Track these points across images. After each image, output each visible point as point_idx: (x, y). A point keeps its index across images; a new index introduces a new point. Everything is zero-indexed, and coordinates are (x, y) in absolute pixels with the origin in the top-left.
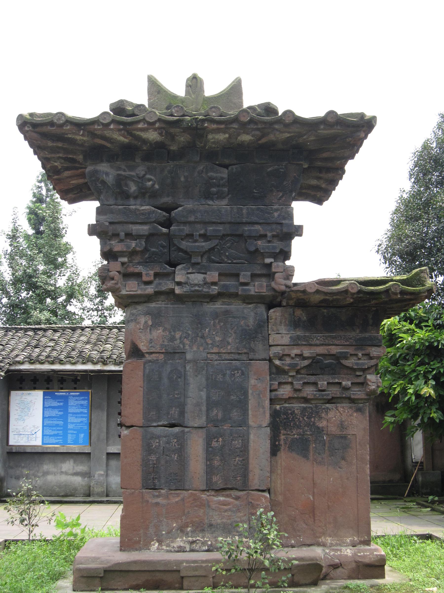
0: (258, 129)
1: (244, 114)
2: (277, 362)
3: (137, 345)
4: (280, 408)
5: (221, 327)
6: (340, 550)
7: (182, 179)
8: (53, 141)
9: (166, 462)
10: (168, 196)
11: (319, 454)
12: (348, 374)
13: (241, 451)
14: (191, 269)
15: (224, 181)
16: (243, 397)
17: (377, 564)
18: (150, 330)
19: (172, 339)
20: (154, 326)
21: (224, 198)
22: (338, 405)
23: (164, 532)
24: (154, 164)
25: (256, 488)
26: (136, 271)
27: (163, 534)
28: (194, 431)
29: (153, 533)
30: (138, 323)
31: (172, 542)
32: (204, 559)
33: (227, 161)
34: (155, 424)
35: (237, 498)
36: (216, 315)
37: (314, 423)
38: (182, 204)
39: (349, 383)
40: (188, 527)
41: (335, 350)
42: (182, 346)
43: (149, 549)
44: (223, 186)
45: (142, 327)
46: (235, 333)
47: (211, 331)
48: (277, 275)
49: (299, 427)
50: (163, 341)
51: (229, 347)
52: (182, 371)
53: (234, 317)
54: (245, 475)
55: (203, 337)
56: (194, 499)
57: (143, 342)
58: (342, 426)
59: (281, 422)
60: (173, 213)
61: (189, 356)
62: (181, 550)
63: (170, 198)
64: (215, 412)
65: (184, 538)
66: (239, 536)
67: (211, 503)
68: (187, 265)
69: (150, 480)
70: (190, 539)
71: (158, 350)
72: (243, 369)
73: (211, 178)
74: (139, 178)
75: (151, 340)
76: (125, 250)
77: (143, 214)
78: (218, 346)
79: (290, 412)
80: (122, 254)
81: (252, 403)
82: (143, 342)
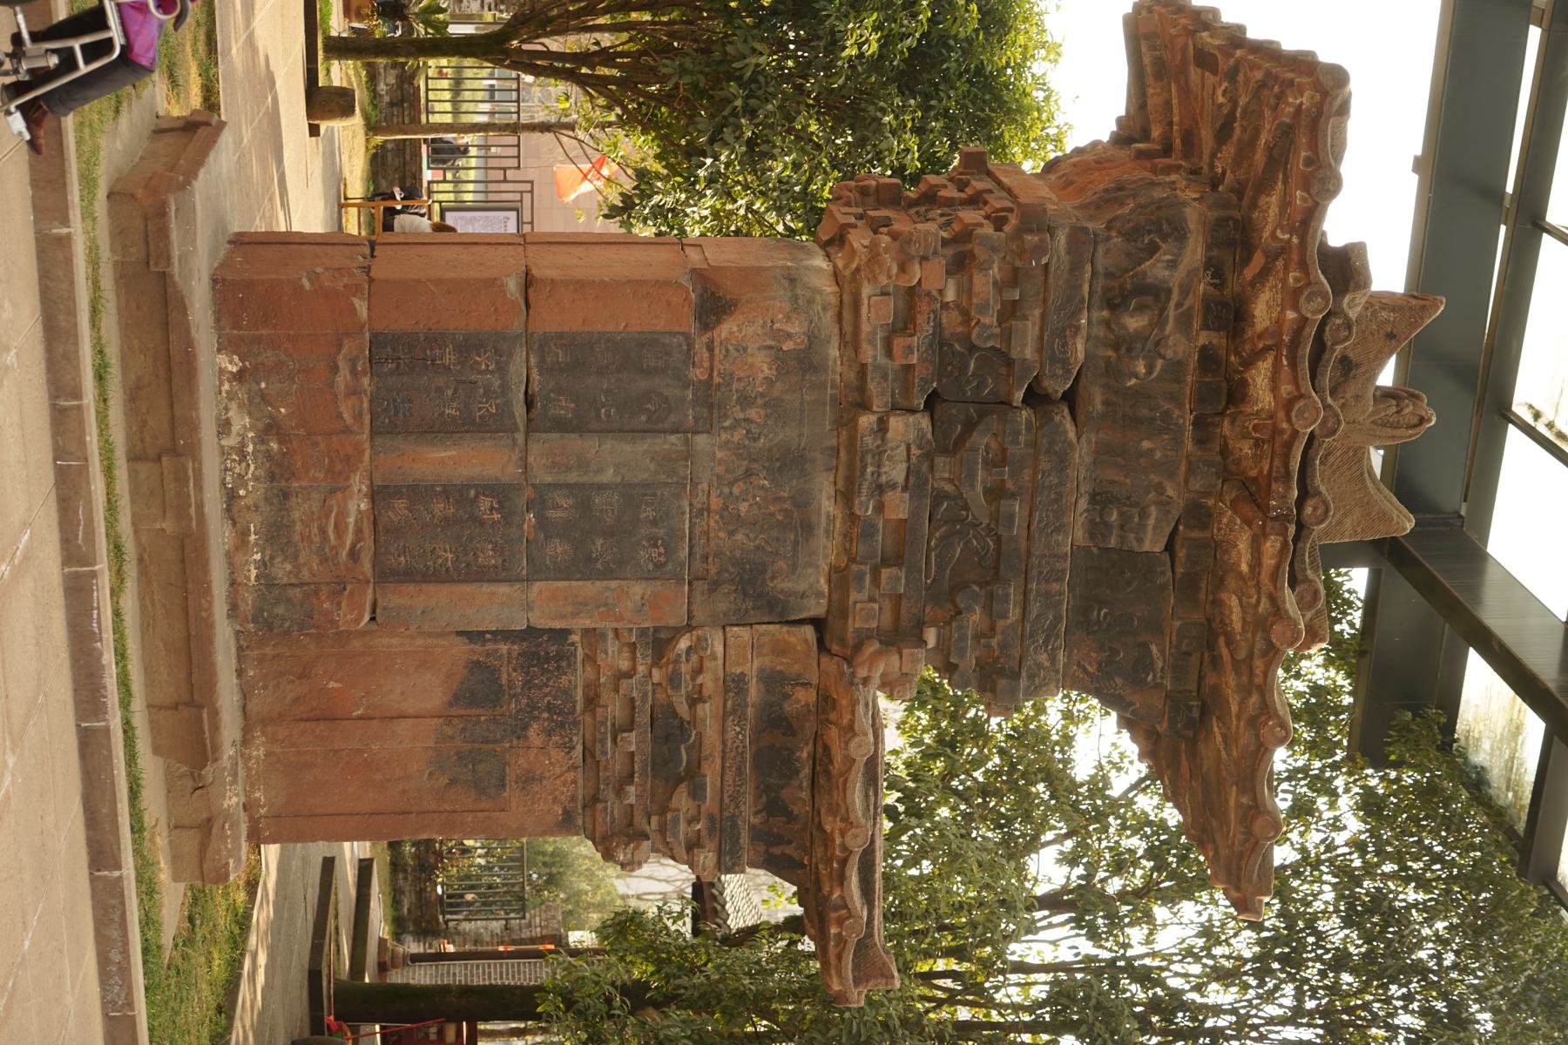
0: (1251, 656)
1: (1289, 634)
2: (684, 644)
3: (732, 313)
4: (573, 644)
5: (773, 515)
6: (234, 782)
7: (1146, 444)
8: (1270, 149)
9: (439, 390)
10: (1105, 403)
11: (463, 730)
12: (653, 795)
13: (468, 565)
14: (918, 452)
15: (1134, 543)
16: (599, 565)
17: (170, 290)
18: (771, 347)
19: (745, 401)
20: (780, 359)
21: (1092, 536)
22: (580, 770)
23: (263, 385)
24: (1189, 379)
25: (380, 603)
26: (920, 319)
27: (259, 384)
28: (515, 456)
29: (260, 359)
30: (788, 318)
31: (240, 406)
32: (206, 510)
33: (1182, 554)
34: (532, 361)
35: (354, 555)
36: (803, 502)
37: (536, 719)
38: (1083, 439)
39: (632, 800)
40: (280, 443)
41: (711, 774)
42: (727, 424)
43: (219, 351)
44: (1122, 539)
45: (777, 326)
46: (757, 548)
47: (761, 493)
48: (894, 659)
49: (528, 685)
50: (739, 379)
51: (722, 535)
52: (666, 425)
53: (796, 543)
54: (408, 576)
55: (748, 474)
56: (348, 458)
57: (740, 331)
58: (528, 780)
59: (540, 645)
60: (1063, 417)
61: (701, 441)
62: (224, 427)
63: (1099, 406)
64: (564, 503)
65: (250, 435)
66: (263, 559)
67: (339, 495)
68: (929, 442)
69: (394, 350)
70: (250, 448)
71: (718, 366)
72: (670, 567)
73: (1144, 514)
74: (1157, 344)
75: (745, 350)
76: (975, 300)
77: (1065, 344)
78: (725, 508)
79: (564, 664)
80: (966, 290)
81: (589, 588)
82: (740, 331)
